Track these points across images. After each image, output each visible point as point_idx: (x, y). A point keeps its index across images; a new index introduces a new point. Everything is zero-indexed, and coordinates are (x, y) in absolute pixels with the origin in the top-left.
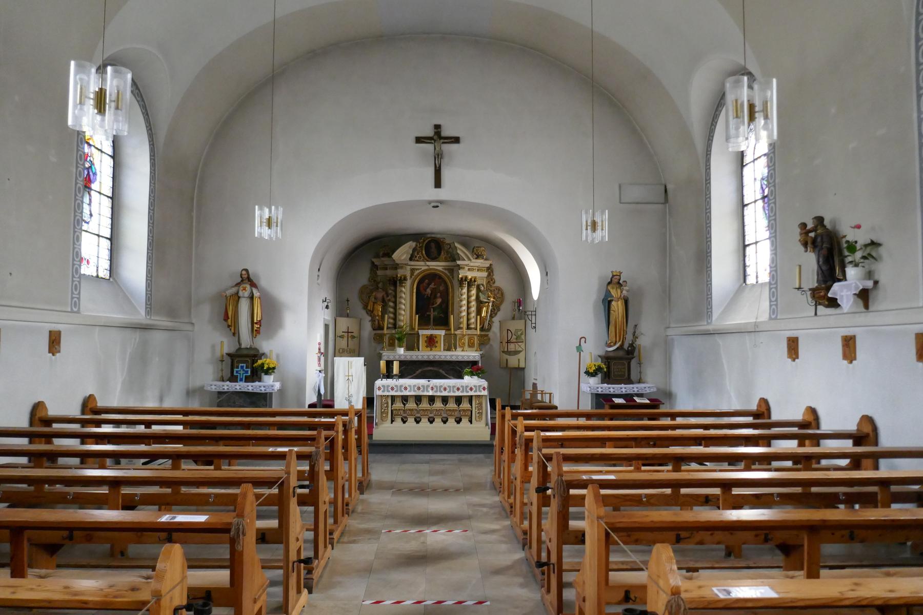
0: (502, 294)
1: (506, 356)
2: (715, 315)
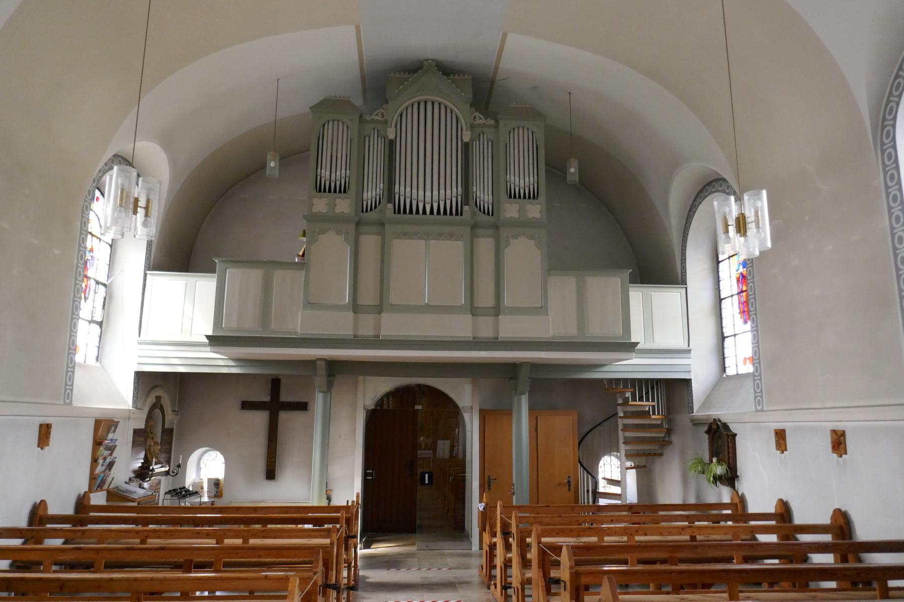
2: (696, 406)
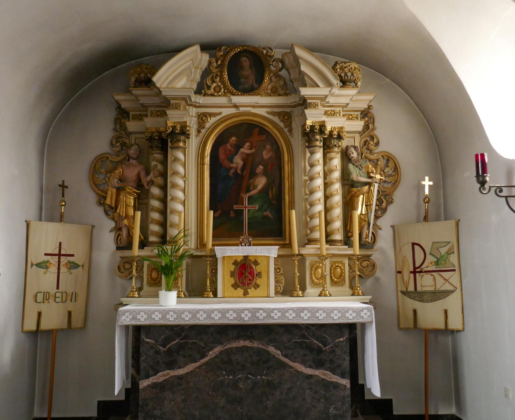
0: (396, 169)
1: (412, 304)
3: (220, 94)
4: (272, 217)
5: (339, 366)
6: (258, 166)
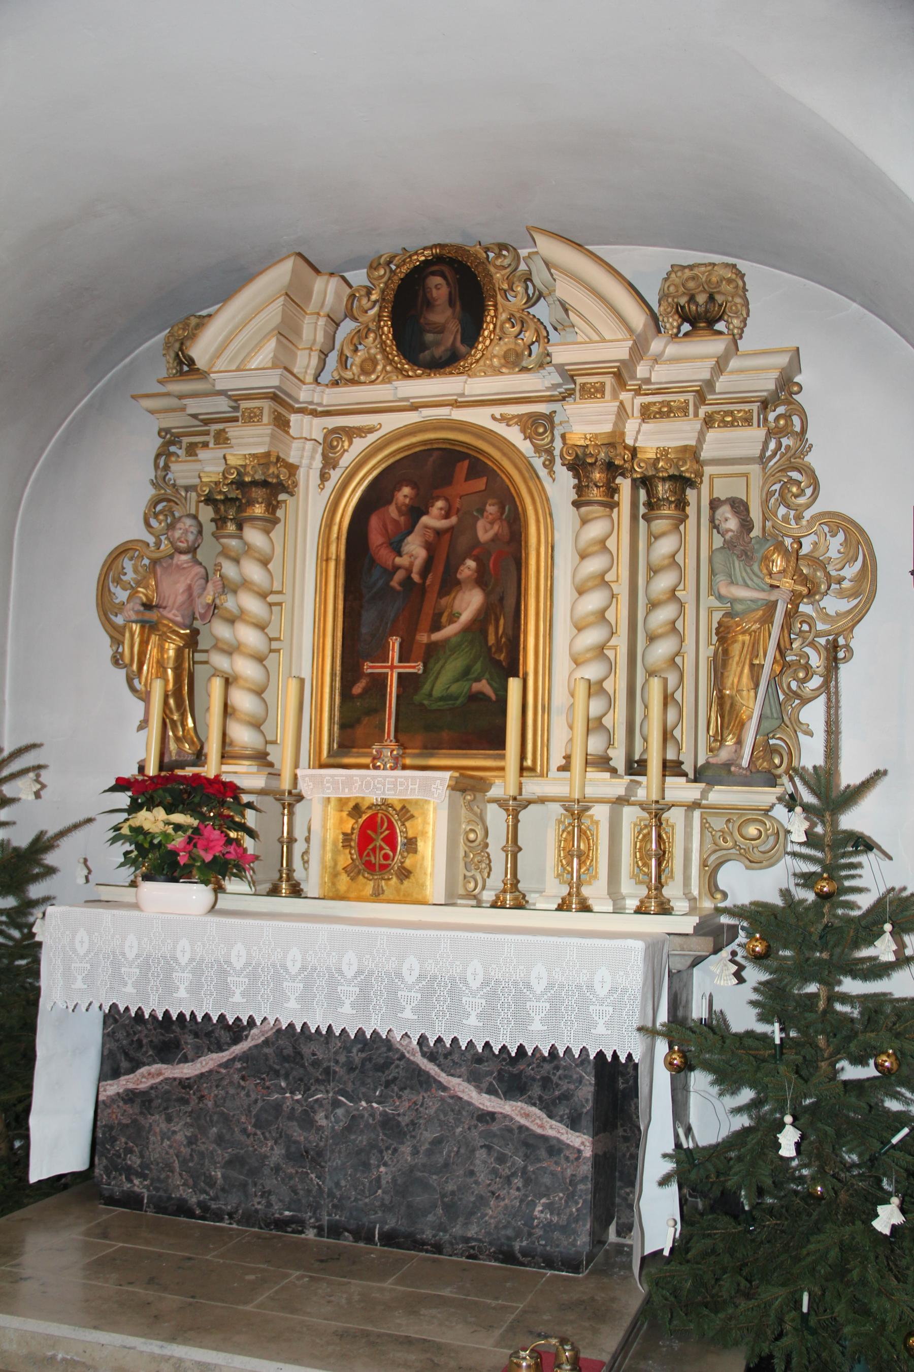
3: (373, 377)
4: (493, 697)
5: (566, 1097)
6: (462, 562)
